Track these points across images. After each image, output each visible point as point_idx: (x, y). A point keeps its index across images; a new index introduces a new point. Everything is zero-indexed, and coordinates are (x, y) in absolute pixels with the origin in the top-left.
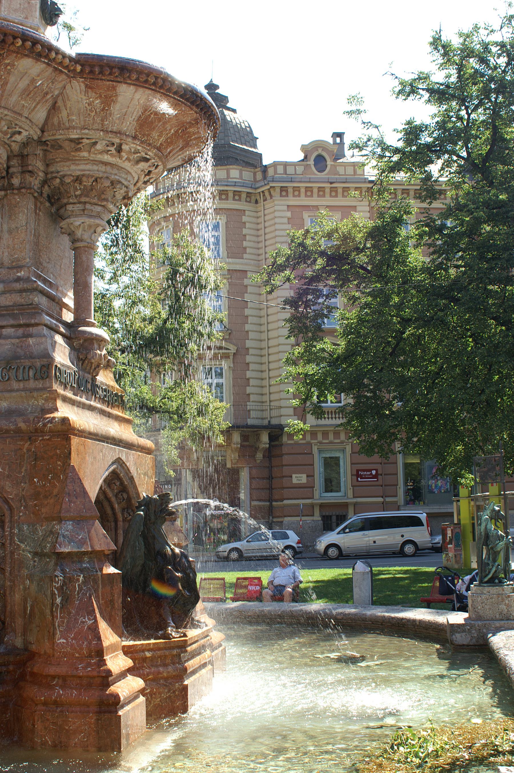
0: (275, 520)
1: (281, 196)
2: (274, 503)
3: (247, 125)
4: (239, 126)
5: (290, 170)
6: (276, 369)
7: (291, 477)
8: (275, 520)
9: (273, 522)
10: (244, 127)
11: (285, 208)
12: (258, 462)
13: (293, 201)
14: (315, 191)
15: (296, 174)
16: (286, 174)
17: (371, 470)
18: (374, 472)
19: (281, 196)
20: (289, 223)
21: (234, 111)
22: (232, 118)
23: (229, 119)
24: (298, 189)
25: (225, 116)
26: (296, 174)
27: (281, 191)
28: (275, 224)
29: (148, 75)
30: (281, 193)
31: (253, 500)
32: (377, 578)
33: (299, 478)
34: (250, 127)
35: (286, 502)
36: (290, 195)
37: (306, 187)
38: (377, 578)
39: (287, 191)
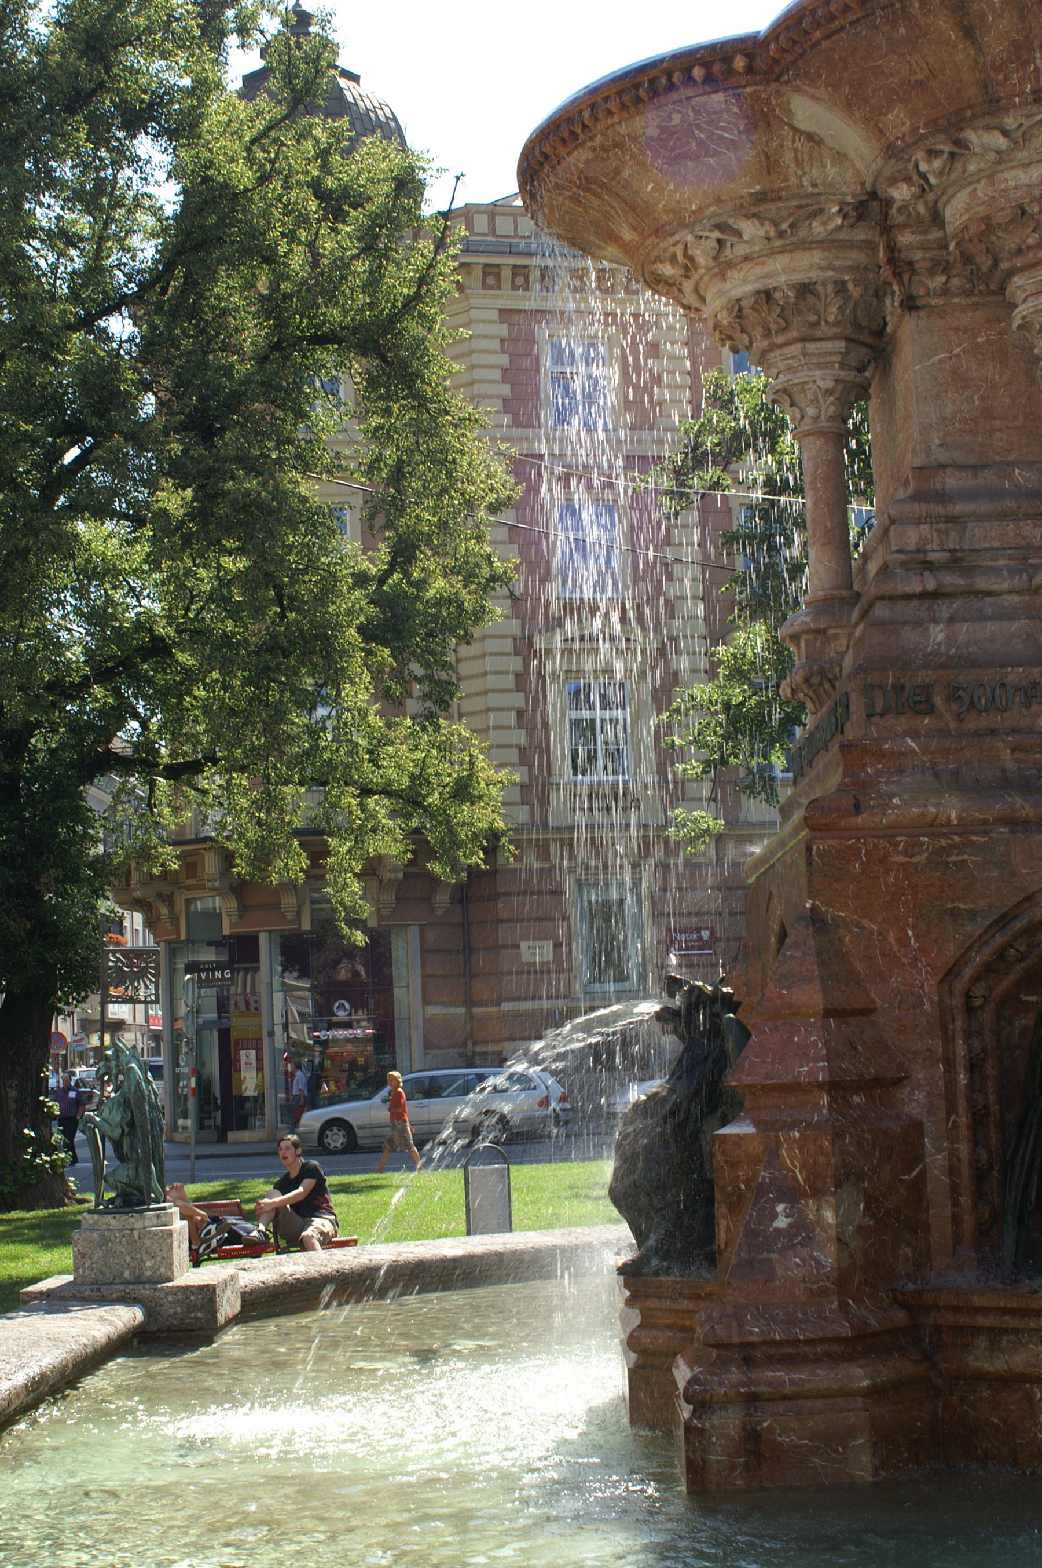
0: (479, 1049)
1: (485, 286)
2: (477, 1010)
3: (389, 115)
4: (372, 115)
5: (504, 226)
6: (478, 694)
7: (518, 947)
8: (479, 1049)
9: (474, 1053)
10: (383, 119)
11: (495, 315)
12: (440, 912)
13: (508, 299)
14: (506, 274)
15: (516, 236)
16: (494, 235)
17: (698, 930)
18: (705, 934)
19: (485, 286)
20: (503, 352)
21: (355, 78)
22: (357, 97)
23: (351, 100)
24: (522, 271)
25: (341, 90)
26: (516, 236)
27: (485, 275)
28: (472, 352)
29: (728, 60)
30: (513, 282)
31: (430, 1003)
32: (30, 1289)
33: (536, 952)
34: (395, 119)
35: (506, 1006)
36: (506, 284)
37: (515, 266)
38: (30, 1289)
39: (498, 276)
